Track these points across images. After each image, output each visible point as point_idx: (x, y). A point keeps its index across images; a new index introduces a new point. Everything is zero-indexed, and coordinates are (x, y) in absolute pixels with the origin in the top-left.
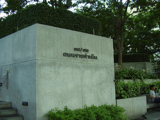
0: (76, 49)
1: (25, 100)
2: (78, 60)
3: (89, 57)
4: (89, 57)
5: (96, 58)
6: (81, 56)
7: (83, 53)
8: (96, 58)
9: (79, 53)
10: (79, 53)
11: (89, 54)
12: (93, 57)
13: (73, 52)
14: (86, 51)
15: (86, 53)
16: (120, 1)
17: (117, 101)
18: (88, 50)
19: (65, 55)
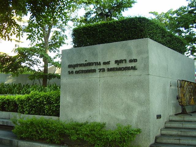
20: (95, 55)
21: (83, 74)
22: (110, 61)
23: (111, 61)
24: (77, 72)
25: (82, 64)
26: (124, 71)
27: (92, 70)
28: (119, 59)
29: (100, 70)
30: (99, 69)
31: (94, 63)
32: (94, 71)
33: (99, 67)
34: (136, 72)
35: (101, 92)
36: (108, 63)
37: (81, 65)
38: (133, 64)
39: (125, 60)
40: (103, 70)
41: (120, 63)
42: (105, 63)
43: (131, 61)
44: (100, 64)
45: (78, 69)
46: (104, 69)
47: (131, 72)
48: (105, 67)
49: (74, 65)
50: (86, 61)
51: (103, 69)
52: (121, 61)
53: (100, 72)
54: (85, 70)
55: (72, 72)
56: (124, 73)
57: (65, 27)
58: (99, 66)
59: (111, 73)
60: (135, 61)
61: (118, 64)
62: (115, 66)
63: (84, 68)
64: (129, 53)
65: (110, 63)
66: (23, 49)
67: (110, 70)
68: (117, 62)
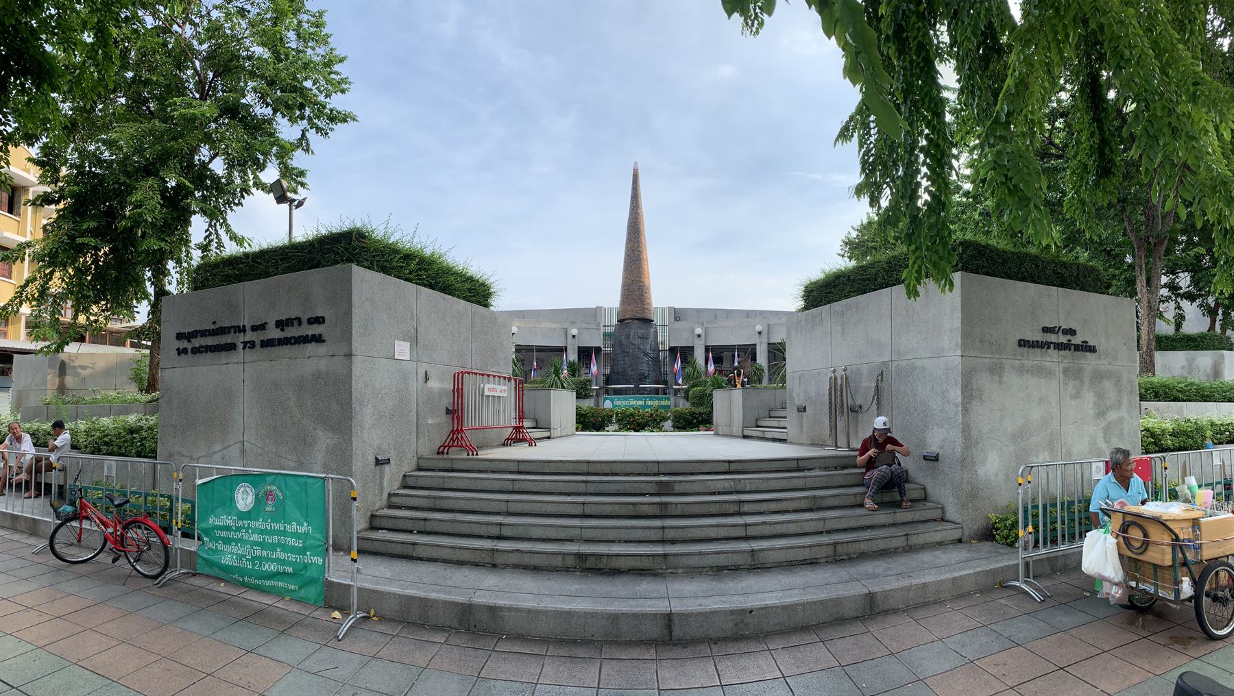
0: (1046, 330)
1: (933, 448)
2: (1052, 359)
3: (1077, 348)
4: (1077, 348)
5: (1092, 349)
6: (1059, 346)
7: (1063, 339)
8: (1092, 349)
9: (1052, 338)
10: (1052, 338)
11: (1077, 340)
12: (1086, 348)
13: (1039, 337)
14: (1072, 332)
15: (1069, 337)
16: (10, 642)
17: (353, 656)
18: (1020, 345)
19: (1023, 343)
24: (196, 351)
28: (284, 318)
29: (245, 343)
32: (231, 347)
34: (321, 349)
37: (204, 333)
40: (252, 345)
42: (255, 328)
44: (244, 330)
45: (197, 342)
47: (311, 348)
48: (256, 337)
55: (185, 351)
60: (318, 320)
61: (283, 330)
62: (275, 333)
63: (210, 341)
67: (266, 344)
68: (280, 324)
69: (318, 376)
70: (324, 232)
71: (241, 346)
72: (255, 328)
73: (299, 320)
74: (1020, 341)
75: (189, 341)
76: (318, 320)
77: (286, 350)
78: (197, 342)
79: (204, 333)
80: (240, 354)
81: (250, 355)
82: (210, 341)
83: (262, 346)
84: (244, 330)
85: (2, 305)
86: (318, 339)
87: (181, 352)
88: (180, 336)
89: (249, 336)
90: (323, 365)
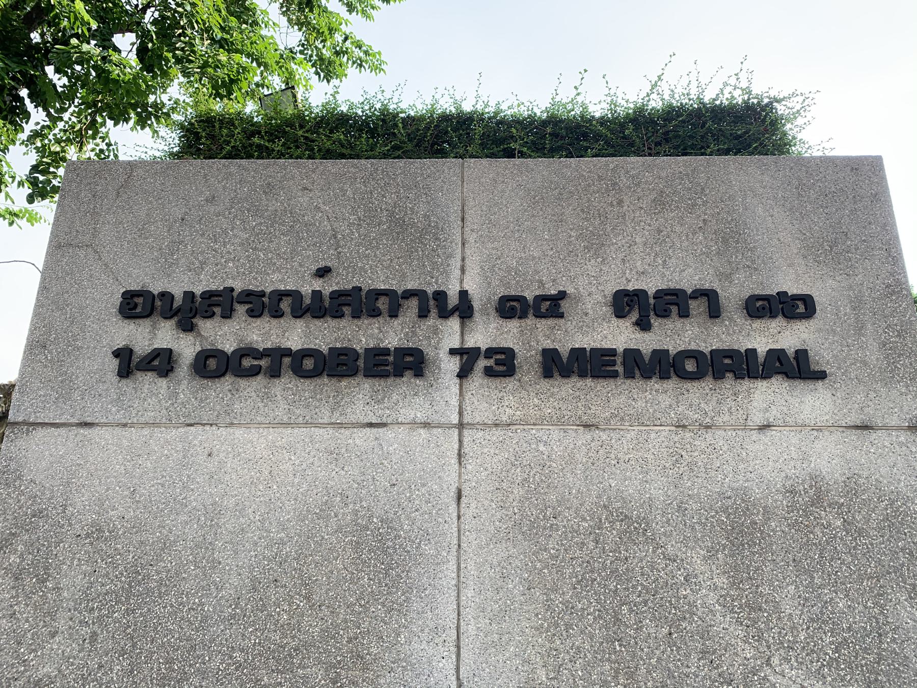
20: (420, 236)
21: (286, 388)
22: (562, 295)
23: (570, 290)
24: (213, 366)
25: (280, 295)
26: (707, 384)
27: (386, 352)
28: (651, 286)
29: (467, 358)
30: (453, 352)
31: (409, 294)
32: (410, 363)
33: (451, 333)
34: (810, 402)
35: (470, 567)
36: (551, 306)
37: (262, 304)
38: (785, 336)
39: (710, 297)
40: (502, 364)
41: (664, 314)
42: (510, 308)
43: (765, 307)
44: (464, 309)
45: (225, 334)
46: (509, 353)
47: (767, 396)
48: (525, 338)
49: (189, 296)
50: (323, 272)
51: (490, 352)
52: (672, 303)
53: (463, 374)
54: (306, 353)
55: (162, 363)
56: (698, 398)
57: (99, 51)
58: (454, 323)
59: (568, 392)
60: (795, 307)
61: (643, 325)
62: (620, 336)
63: (295, 335)
64: (731, 239)
65: (565, 305)
66: (885, 225)
67: (555, 365)
68: (626, 303)
69: (811, 498)
70: (446, 106)
71: (452, 365)
72: (510, 308)
73: (710, 300)
74: (505, 299)
75: (187, 326)
76: (795, 307)
77: (659, 396)
78: (225, 334)
79: (262, 304)
80: (444, 392)
81: (486, 399)
82: (295, 335)
83: (547, 374)
84: (464, 309)
85: (5, 381)
86: (797, 368)
87: (128, 363)
88: (137, 305)
89: (485, 333)
90: (829, 457)
